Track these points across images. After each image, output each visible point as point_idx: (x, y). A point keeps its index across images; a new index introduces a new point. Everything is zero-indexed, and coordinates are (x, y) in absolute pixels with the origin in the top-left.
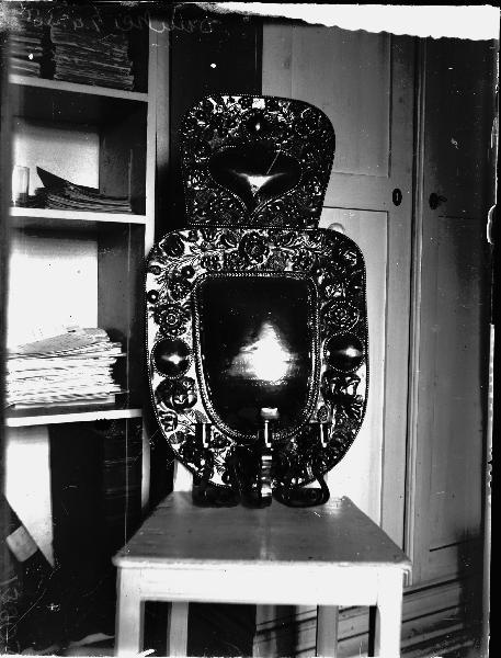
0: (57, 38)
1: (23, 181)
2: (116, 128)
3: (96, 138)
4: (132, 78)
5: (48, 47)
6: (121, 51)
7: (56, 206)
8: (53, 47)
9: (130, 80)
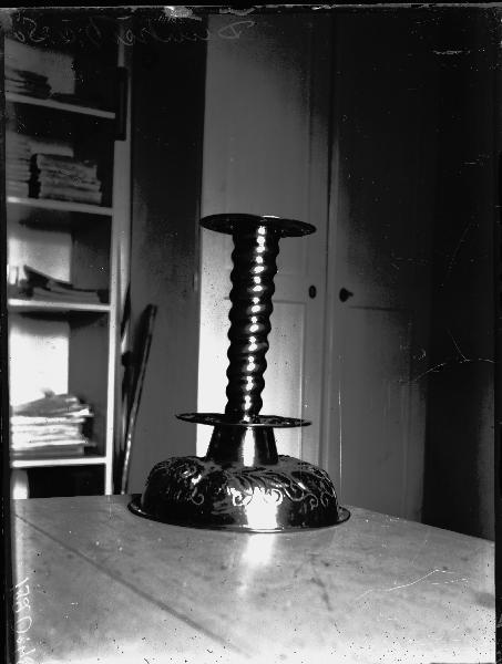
0: (43, 164)
1: (15, 274)
2: (89, 235)
3: (68, 237)
4: (100, 194)
5: (35, 171)
6: (91, 173)
7: (39, 298)
8: (39, 171)
9: (98, 197)
